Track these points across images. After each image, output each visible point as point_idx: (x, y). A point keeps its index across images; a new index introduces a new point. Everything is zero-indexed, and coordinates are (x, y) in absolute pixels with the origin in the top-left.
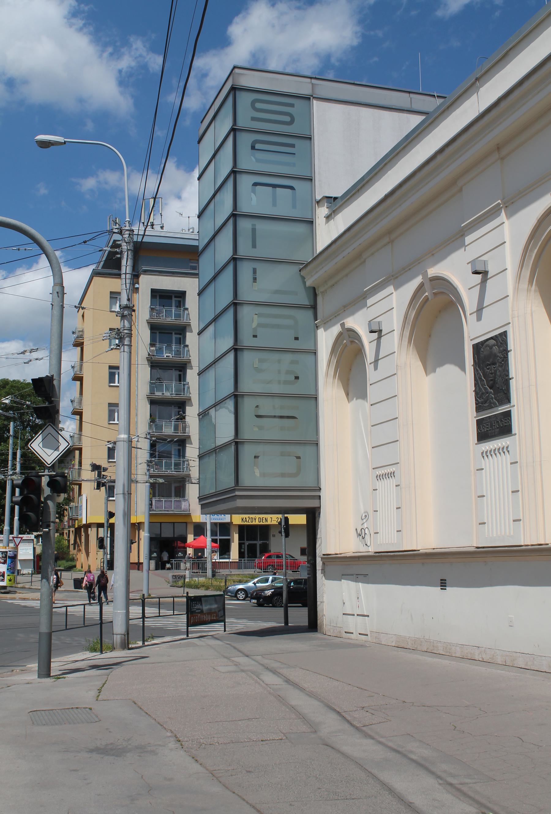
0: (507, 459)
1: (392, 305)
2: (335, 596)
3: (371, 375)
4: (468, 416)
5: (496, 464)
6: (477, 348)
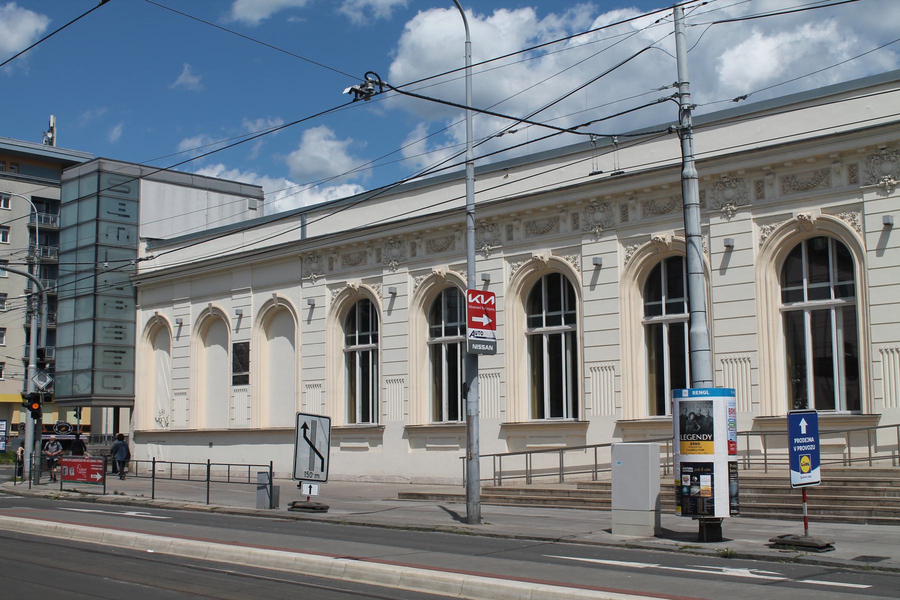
0: (246, 394)
1: (192, 312)
2: (140, 452)
3: (174, 343)
4: (229, 374)
5: (240, 395)
6: (235, 345)
